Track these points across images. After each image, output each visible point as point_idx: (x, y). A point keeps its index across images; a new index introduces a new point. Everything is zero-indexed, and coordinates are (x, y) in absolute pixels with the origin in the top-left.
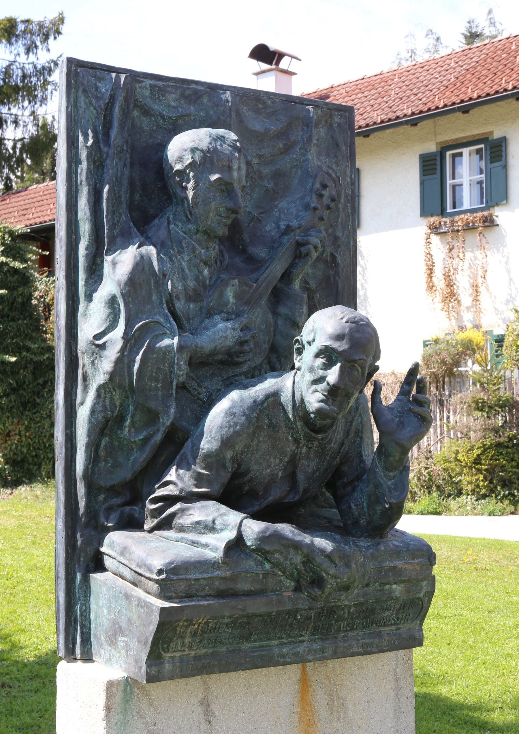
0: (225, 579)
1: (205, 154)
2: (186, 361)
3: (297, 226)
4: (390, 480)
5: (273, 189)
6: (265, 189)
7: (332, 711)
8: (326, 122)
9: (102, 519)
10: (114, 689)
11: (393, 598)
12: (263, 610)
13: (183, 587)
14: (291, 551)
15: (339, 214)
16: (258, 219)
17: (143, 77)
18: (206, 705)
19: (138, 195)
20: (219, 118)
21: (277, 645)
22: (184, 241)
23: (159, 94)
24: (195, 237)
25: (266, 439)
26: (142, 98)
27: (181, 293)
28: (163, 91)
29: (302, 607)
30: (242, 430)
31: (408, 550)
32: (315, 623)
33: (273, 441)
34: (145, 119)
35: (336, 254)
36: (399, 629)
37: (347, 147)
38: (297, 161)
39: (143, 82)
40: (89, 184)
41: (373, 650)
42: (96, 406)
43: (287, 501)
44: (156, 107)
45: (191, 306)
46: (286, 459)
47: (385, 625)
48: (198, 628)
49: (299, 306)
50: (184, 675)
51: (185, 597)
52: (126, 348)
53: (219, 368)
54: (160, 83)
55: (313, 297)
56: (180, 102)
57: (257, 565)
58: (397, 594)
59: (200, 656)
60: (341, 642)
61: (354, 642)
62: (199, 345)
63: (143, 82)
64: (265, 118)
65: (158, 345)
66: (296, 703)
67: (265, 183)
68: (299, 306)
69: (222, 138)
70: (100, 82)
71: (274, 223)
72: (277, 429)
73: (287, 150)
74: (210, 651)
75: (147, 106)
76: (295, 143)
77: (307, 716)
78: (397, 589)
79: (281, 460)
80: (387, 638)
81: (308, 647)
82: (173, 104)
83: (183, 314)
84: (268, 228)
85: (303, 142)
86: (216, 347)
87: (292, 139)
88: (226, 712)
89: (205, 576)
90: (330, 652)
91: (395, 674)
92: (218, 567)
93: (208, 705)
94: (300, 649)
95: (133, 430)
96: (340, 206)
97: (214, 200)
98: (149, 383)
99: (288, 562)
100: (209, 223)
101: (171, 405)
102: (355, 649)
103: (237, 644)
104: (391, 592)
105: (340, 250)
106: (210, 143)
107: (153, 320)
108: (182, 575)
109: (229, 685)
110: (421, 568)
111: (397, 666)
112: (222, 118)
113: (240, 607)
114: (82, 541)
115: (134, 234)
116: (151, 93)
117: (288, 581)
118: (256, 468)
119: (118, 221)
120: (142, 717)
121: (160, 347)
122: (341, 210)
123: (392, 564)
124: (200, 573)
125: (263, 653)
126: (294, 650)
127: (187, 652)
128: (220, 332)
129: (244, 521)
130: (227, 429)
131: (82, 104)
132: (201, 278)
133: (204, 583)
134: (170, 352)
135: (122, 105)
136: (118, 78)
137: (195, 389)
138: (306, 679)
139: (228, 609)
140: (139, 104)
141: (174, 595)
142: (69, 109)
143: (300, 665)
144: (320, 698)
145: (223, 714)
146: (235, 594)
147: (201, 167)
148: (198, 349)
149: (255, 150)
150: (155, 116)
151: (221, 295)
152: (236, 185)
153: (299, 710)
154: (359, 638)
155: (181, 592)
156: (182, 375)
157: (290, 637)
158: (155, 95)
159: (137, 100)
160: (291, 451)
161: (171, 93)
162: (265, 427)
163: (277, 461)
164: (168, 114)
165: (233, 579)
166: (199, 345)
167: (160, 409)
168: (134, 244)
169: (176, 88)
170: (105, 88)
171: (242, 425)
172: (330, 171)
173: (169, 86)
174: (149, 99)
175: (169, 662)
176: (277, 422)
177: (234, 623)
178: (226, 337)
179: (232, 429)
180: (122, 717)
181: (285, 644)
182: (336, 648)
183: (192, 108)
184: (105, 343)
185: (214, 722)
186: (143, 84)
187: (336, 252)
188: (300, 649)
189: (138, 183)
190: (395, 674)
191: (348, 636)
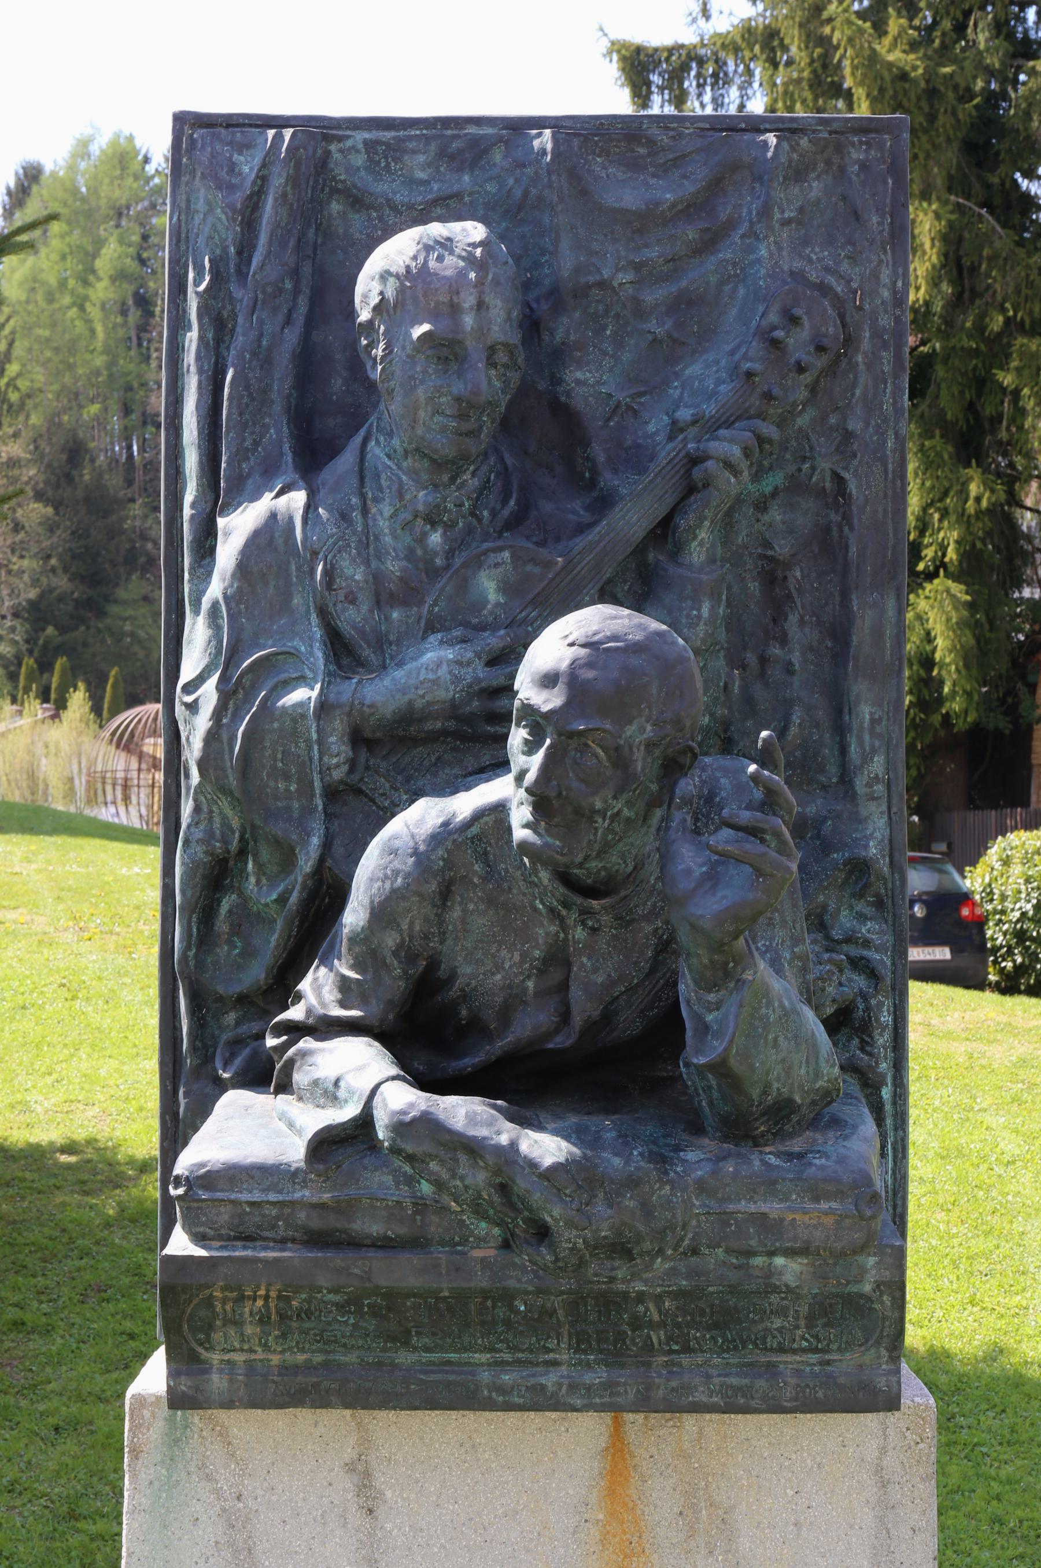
0: (321, 1206)
1: (402, 284)
2: (343, 736)
3: (689, 418)
4: (710, 1011)
5: (670, 337)
6: (650, 337)
7: (692, 1532)
8: (828, 163)
9: (218, 1063)
10: (147, 1413)
11: (776, 1287)
12: (414, 1282)
13: (226, 1217)
14: (463, 1158)
15: (856, 378)
16: (629, 407)
17: (347, 128)
18: (362, 1474)
19: (340, 381)
20: (526, 193)
21: (489, 1365)
22: (383, 476)
23: (386, 158)
24: (405, 464)
25: (482, 907)
26: (347, 173)
27: (361, 589)
28: (395, 151)
29: (518, 1286)
30: (406, 886)
31: (800, 1179)
32: (572, 1324)
33: (502, 913)
34: (357, 216)
35: (846, 476)
36: (828, 1363)
37: (882, 216)
38: (735, 265)
39: (348, 137)
40: (200, 371)
41: (753, 1403)
42: (192, 830)
43: (551, 1046)
44: (381, 188)
45: (395, 615)
46: (537, 953)
47: (781, 1350)
48: (266, 1305)
49: (689, 603)
50: (255, 1403)
51: (236, 1238)
52: (226, 709)
53: (455, 749)
54: (389, 135)
55: (785, 578)
56: (438, 168)
57: (397, 1184)
58: (789, 1279)
59: (297, 1366)
60: (660, 1375)
61: (697, 1381)
62: (367, 702)
63: (348, 137)
64: (654, 176)
65: (280, 704)
66: (594, 1498)
67: (652, 325)
68: (689, 603)
69: (446, 244)
70: (240, 154)
71: (667, 414)
72: (505, 885)
73: (710, 242)
74: (318, 1358)
75: (359, 189)
76: (731, 225)
77: (624, 1533)
78: (789, 1269)
79: (524, 956)
80: (792, 1381)
81: (569, 1377)
82: (421, 175)
83: (362, 633)
84: (651, 428)
85: (751, 221)
86: (410, 703)
87: (723, 216)
88: (413, 1496)
89: (272, 1197)
90: (631, 1396)
91: (879, 1470)
92: (304, 1181)
93: (367, 1474)
94: (549, 1380)
95: (264, 881)
96: (860, 358)
97: (422, 382)
98: (272, 783)
99: (458, 1183)
100: (419, 432)
101: (313, 829)
102: (700, 1397)
103: (385, 1350)
104: (769, 1272)
105: (856, 462)
106: (415, 258)
107: (284, 649)
108: (221, 1191)
109: (421, 1438)
110: (838, 1223)
111: (883, 1450)
112: (534, 191)
113: (356, 1271)
114: (187, 1104)
115: (284, 466)
116: (370, 159)
117: (483, 1225)
118: (469, 970)
119: (256, 443)
120: (209, 1478)
121: (283, 707)
122: (862, 367)
123: (752, 1208)
124: (263, 1191)
125: (451, 1377)
126: (532, 1381)
127: (260, 1355)
128: (423, 671)
129: (383, 1087)
130: (380, 883)
131: (201, 206)
132: (419, 552)
133: (274, 1212)
134: (303, 716)
135: (284, 195)
136: (278, 137)
137: (384, 794)
138: (621, 1450)
139: (329, 1273)
140: (340, 186)
141: (211, 1233)
142: (175, 219)
143: (608, 1417)
144: (660, 1497)
145: (403, 1499)
146: (354, 1243)
147: (398, 312)
148: (365, 709)
149: (623, 253)
150: (378, 208)
151: (464, 586)
152: (470, 343)
153: (601, 1516)
154: (715, 1372)
155: (222, 1226)
156: (337, 766)
157: (516, 1349)
158: (379, 162)
159: (334, 178)
160: (547, 934)
161: (414, 152)
162: (476, 880)
163: (517, 957)
164: (406, 200)
165: (345, 1208)
166: (367, 702)
167: (294, 837)
168: (271, 491)
169: (427, 139)
170: (248, 166)
171: (408, 875)
172: (831, 280)
173: (411, 138)
174: (363, 173)
175: (221, 1371)
176: (507, 871)
177: (352, 1304)
178: (435, 682)
179: (388, 885)
180: (164, 1471)
181: (508, 1363)
182: (649, 1387)
183: (466, 178)
184: (196, 701)
185: (381, 1511)
186: (349, 143)
187: (846, 468)
188: (549, 1380)
189: (338, 356)
190: (879, 1470)
191: (680, 1365)
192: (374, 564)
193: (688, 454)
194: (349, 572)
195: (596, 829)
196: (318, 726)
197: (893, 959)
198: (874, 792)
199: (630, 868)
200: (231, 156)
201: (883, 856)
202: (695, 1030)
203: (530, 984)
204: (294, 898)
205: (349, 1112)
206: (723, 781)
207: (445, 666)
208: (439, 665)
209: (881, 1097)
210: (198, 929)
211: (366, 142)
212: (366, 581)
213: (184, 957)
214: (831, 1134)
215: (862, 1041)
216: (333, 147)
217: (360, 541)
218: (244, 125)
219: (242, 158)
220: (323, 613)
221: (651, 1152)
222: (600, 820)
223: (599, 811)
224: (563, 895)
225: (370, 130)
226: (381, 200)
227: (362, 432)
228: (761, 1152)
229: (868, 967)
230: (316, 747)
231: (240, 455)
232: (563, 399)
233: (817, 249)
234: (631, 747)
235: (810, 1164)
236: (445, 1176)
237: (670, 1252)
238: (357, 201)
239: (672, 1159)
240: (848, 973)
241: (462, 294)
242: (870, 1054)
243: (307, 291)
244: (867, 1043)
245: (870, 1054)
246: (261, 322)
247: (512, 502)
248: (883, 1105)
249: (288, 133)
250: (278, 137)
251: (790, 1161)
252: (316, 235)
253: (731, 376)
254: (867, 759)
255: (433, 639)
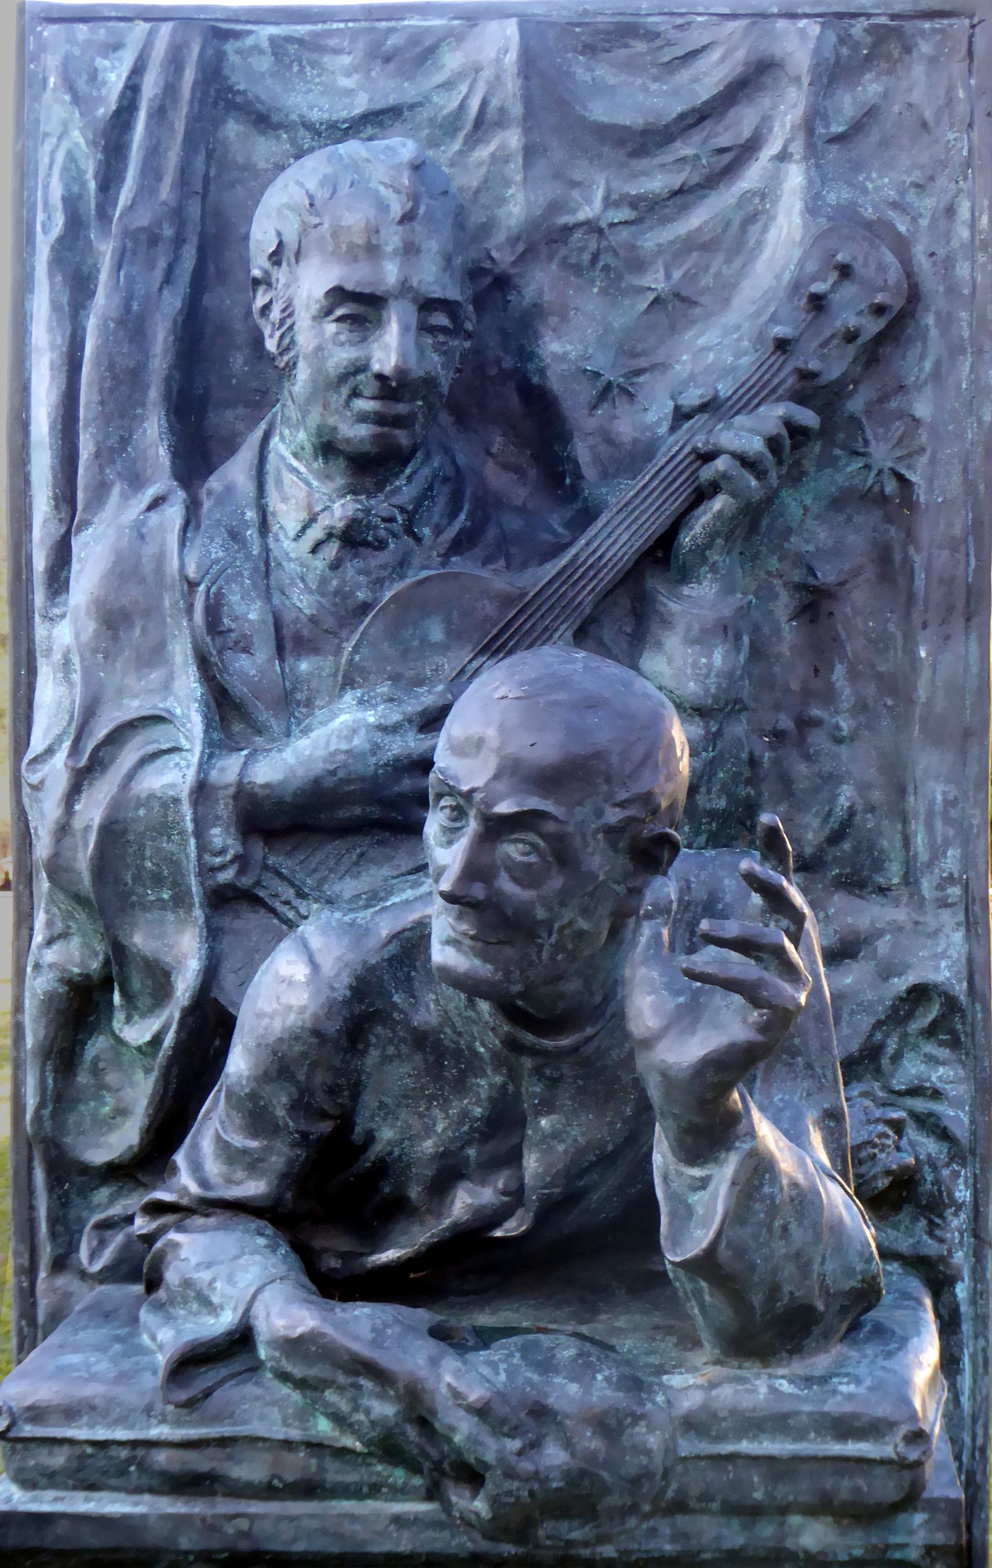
25: (405, 1049)
33: (431, 1059)
39: (249, 33)
43: (498, 1233)
46: (478, 1111)
54: (301, 30)
70: (106, 57)
136: (151, 35)
160: (490, 1085)
161: (337, 51)
169: (354, 35)
173: (330, 33)
184: (42, 782)
186: (250, 41)
192: (276, 599)
193: (694, 450)
194: (240, 609)
195: (541, 946)
196: (195, 813)
197: (972, 1114)
198: (948, 896)
199: (598, 999)
200: (93, 60)
201: (960, 981)
202: (673, 1215)
203: (471, 1152)
204: (169, 1040)
205: (227, 1320)
206: (726, 881)
207: (363, 732)
208: (354, 731)
209: (955, 1296)
210: (55, 1080)
211: (272, 40)
212: (265, 622)
213: (37, 1117)
214: (870, 1350)
215: (931, 1223)
216: (229, 47)
217: (256, 569)
218: (109, 19)
219: (107, 63)
220: (203, 662)
221: (622, 1377)
222: (545, 935)
223: (542, 921)
224: (508, 1034)
225: (277, 23)
226: (294, 117)
227: (263, 426)
228: (770, 1376)
229: (938, 1126)
230: (192, 841)
231: (103, 456)
232: (535, 380)
233: (874, 175)
234: (584, 836)
235: (835, 1392)
236: (344, 1406)
237: (647, 1508)
238: (264, 121)
239: (651, 1384)
240: (912, 1132)
241: (383, 232)
242: (941, 1241)
243: (194, 240)
244: (938, 1225)
245: (941, 1241)
246: (131, 281)
247: (463, 516)
248: (958, 1306)
249: (165, 29)
250: (151, 35)
251: (809, 1388)
252: (208, 165)
253: (754, 346)
254: (937, 854)
255: (350, 697)
